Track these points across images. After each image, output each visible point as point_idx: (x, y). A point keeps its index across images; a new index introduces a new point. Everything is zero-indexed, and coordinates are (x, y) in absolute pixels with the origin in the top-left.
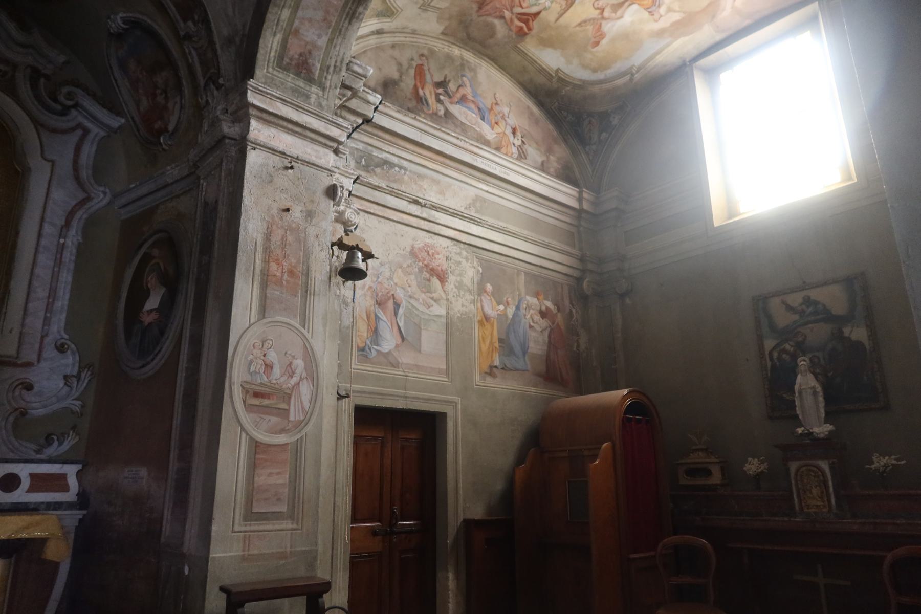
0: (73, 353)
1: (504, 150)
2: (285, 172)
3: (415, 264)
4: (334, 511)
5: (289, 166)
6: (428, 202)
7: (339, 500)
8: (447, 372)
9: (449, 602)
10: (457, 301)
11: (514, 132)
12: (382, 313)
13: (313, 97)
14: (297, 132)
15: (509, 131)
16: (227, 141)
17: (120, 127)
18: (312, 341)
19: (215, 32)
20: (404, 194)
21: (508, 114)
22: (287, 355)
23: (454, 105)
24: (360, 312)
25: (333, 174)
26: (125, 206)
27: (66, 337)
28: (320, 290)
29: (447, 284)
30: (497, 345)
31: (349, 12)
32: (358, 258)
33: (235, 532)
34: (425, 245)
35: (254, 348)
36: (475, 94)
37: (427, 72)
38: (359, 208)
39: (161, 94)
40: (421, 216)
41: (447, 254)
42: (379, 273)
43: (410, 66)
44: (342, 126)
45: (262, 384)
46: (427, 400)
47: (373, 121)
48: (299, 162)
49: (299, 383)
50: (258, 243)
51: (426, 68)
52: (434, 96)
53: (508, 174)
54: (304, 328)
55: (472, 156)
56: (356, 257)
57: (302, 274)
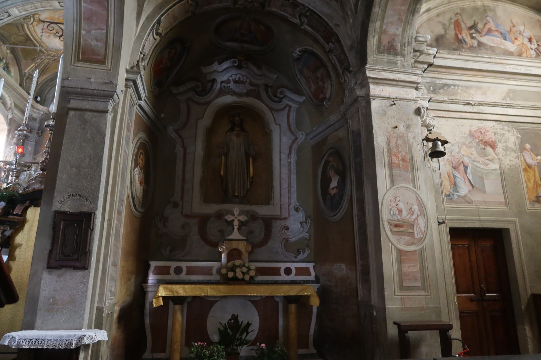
0: (302, 212)
1: (524, 55)
2: (392, 107)
3: (473, 141)
4: (446, 286)
5: (393, 103)
6: (476, 102)
7: (448, 280)
8: (506, 203)
9: (529, 345)
10: (506, 158)
11: (530, 40)
12: (457, 173)
13: (399, 63)
14: (394, 85)
15: (526, 41)
16: (359, 98)
17: (304, 101)
18: (420, 195)
19: (344, 45)
20: (460, 101)
21: (524, 30)
22: (409, 204)
23: (483, 37)
24: (444, 174)
25: (417, 102)
26: (312, 138)
27: (298, 204)
28: (420, 167)
29: (497, 149)
31: (412, 10)
32: (439, 145)
33: (396, 296)
34: (478, 128)
35: (391, 202)
36: (497, 25)
37: (462, 23)
38: (434, 115)
39: (321, 81)
40: (473, 111)
41: (495, 130)
42: (451, 150)
43: (450, 23)
44: (418, 74)
45: (398, 220)
47: (434, 64)
48: (398, 100)
49: (417, 218)
50: (384, 147)
51: (460, 21)
52: (469, 36)
53: (530, 70)
54: (415, 188)
55: (502, 66)
56: (438, 145)
57: (409, 159)
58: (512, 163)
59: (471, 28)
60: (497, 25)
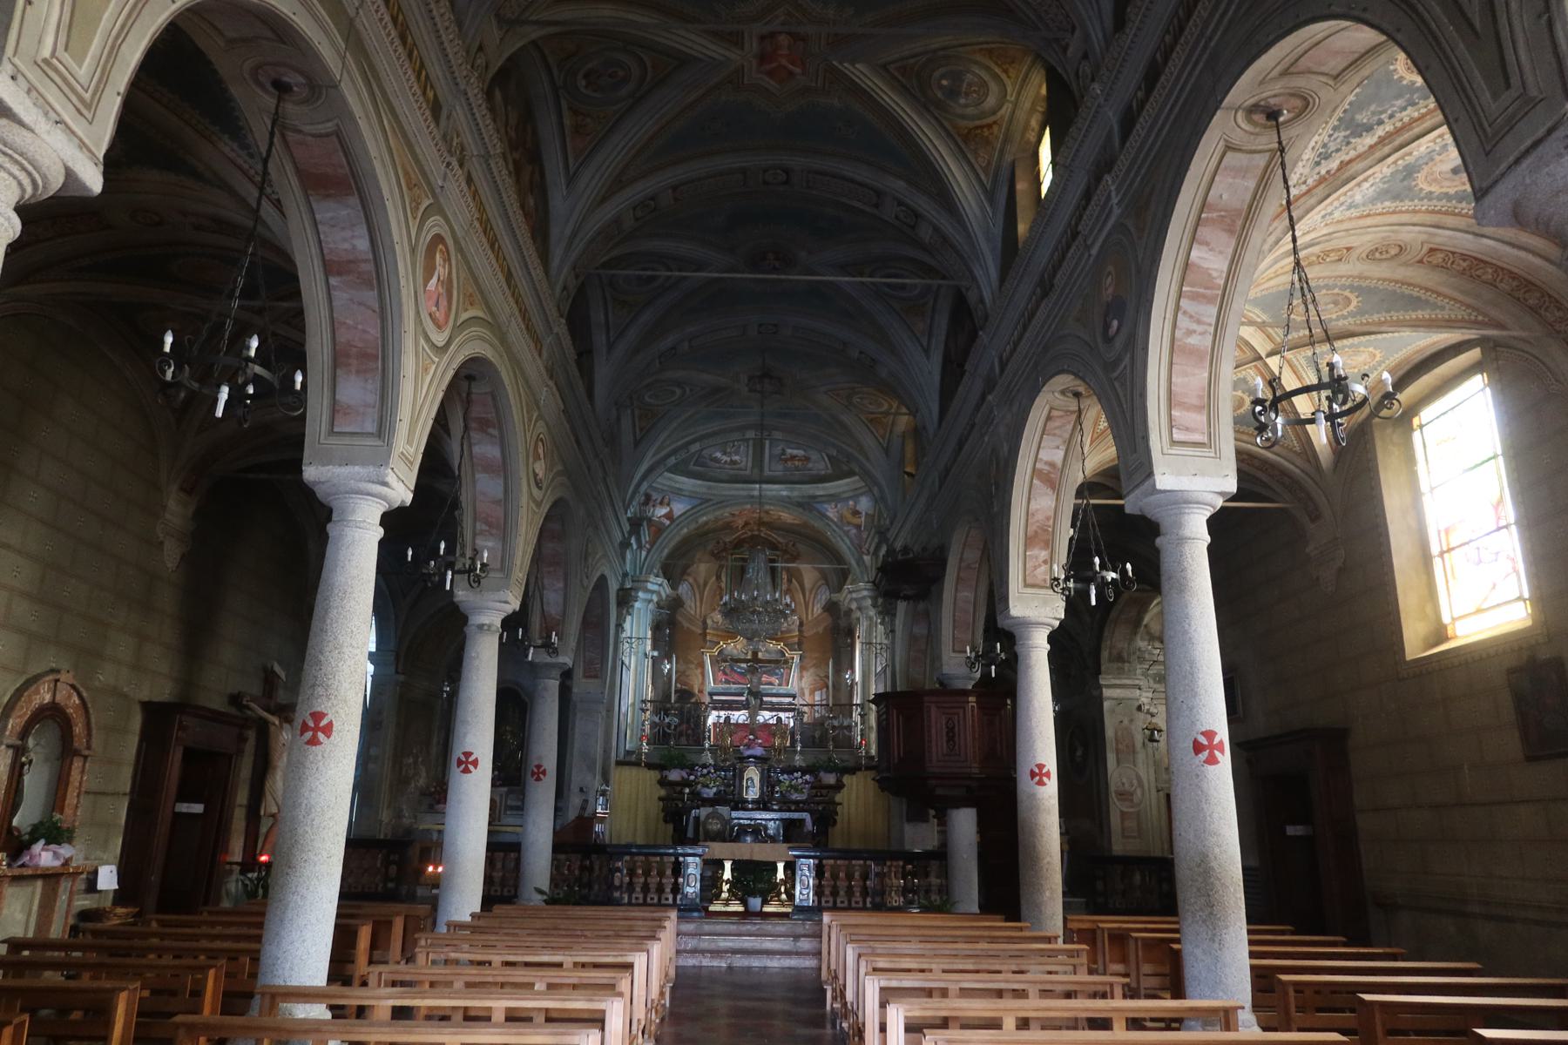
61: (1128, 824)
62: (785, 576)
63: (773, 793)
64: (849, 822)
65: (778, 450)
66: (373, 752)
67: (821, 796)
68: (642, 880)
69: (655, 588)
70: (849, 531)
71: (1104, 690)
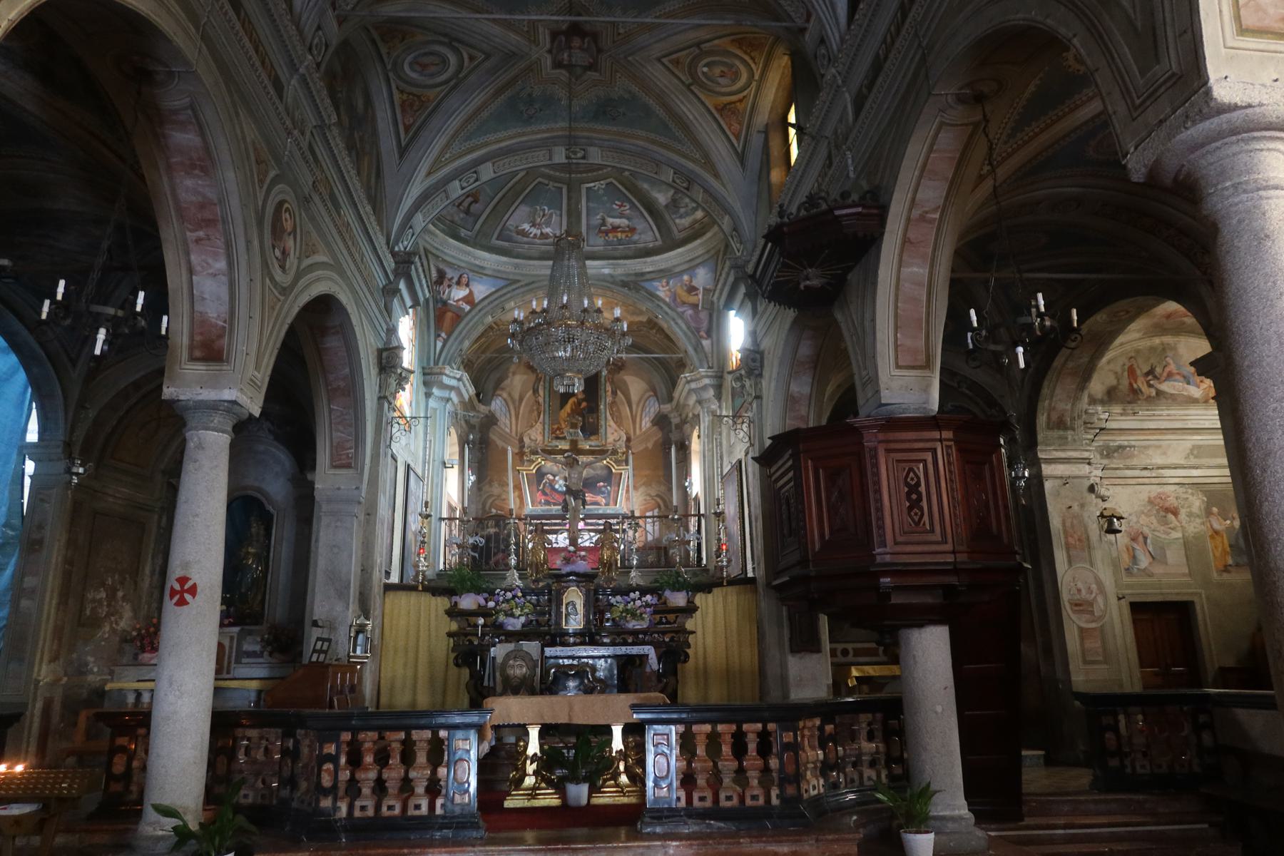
30: (1228, 549)
43: (1123, 371)
46: (1178, 594)
51: (1135, 366)
58: (1196, 530)
59: (1147, 374)
60: (1178, 366)
61: (1089, 644)
62: (609, 388)
63: (602, 622)
64: (705, 658)
65: (596, 220)
66: (29, 582)
67: (668, 623)
68: (372, 775)
69: (453, 383)
70: (683, 313)
71: (1043, 466)
